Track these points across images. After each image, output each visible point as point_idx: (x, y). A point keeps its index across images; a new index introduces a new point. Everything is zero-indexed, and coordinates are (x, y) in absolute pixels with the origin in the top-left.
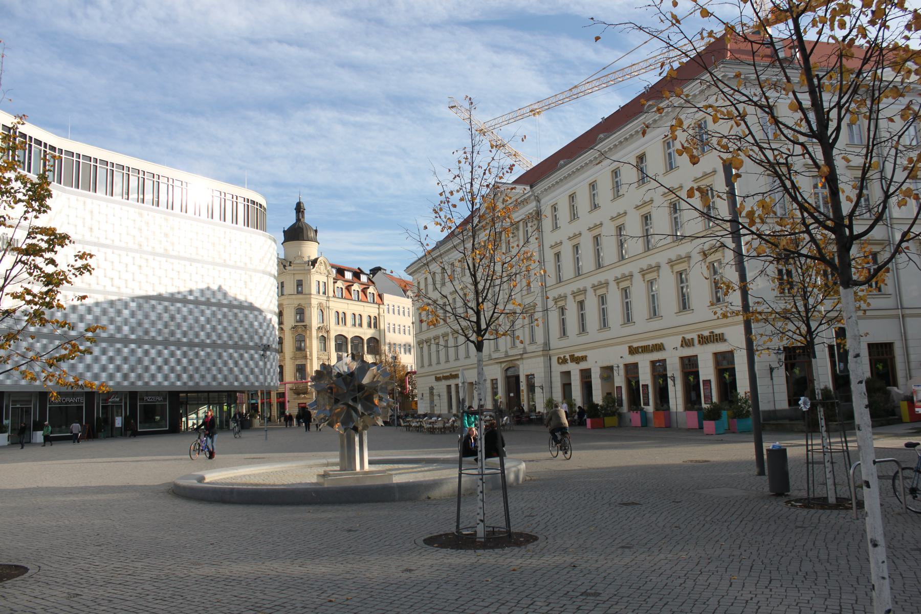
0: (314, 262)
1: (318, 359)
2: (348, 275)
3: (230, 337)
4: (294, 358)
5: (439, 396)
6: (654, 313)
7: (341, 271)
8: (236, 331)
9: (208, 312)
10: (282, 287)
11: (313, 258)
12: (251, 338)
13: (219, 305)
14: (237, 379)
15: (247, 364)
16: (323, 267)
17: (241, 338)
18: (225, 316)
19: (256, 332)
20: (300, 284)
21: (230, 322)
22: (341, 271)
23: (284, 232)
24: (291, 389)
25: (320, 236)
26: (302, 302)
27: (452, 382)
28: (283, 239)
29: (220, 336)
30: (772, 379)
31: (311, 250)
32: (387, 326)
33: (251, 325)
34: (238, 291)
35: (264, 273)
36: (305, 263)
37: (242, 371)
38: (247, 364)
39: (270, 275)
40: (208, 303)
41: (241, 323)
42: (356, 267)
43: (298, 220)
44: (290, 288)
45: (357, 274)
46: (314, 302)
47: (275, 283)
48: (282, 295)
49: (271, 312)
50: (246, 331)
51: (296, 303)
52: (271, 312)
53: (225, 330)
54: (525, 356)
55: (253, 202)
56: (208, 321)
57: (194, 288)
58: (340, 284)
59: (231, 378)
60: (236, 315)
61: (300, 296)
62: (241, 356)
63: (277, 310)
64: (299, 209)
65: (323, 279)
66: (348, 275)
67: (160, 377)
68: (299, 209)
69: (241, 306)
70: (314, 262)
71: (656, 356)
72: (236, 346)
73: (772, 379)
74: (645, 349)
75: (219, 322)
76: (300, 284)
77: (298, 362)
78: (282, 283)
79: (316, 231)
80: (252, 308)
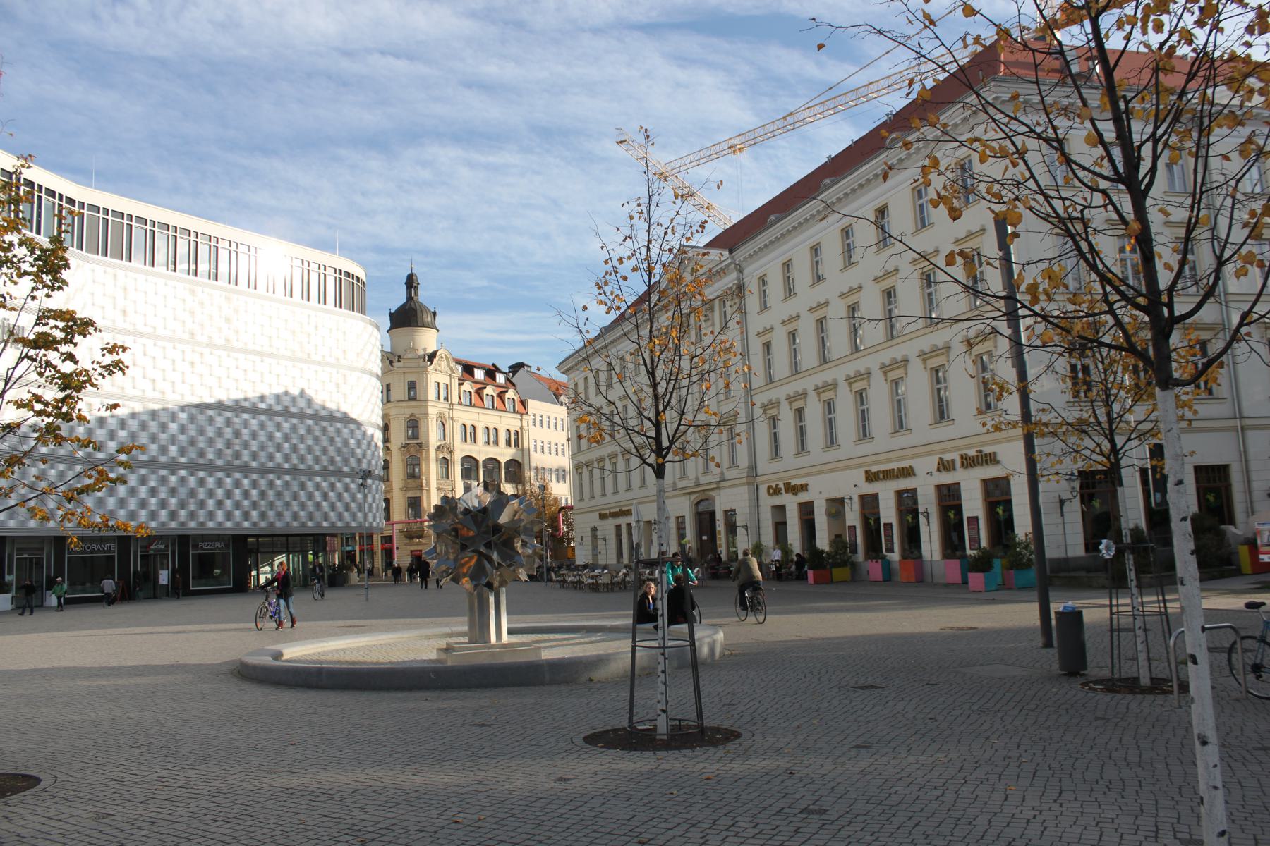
0: (432, 357)
1: (438, 489)
2: (479, 374)
3: (317, 460)
4: (405, 488)
5: (605, 540)
6: (900, 425)
7: (468, 369)
8: (325, 451)
9: (286, 426)
10: (388, 390)
11: (430, 351)
12: (346, 461)
13: (302, 416)
14: (326, 518)
15: (340, 497)
16: (444, 363)
17: (332, 461)
18: (309, 430)
19: (353, 453)
20: (412, 386)
21: (316, 439)
22: (468, 369)
23: (391, 314)
24: (401, 531)
25: (439, 320)
26: (416, 411)
27: (623, 521)
28: (388, 325)
29: (302, 459)
30: (1062, 515)
31: (427, 340)
32: (532, 443)
33: (346, 443)
34: (328, 397)
35: (364, 371)
36: (420, 357)
37: (333, 507)
38: (340, 497)
39: (372, 374)
40: (286, 414)
41: (332, 440)
42: (489, 363)
43: (410, 298)
44: (399, 392)
45: (491, 373)
46: (432, 411)
47: (379, 385)
48: (388, 401)
49: (372, 425)
50: (339, 451)
51: (408, 412)
52: (372, 425)
53: (310, 450)
54: (723, 484)
55: (348, 274)
56: (286, 438)
57: (267, 393)
58: (467, 386)
59: (318, 516)
60: (324, 430)
61: (413, 403)
62: (332, 486)
63: (381, 423)
64: (411, 283)
65: (444, 379)
66: (479, 374)
67: (220, 516)
68: (411, 283)
69: (332, 418)
70: (432, 357)
71: (904, 484)
72: (324, 473)
73: (1062, 515)
74: (888, 475)
75: (302, 439)
76: (412, 386)
77: (411, 494)
78: (388, 385)
79: (434, 314)
80: (346, 419)
